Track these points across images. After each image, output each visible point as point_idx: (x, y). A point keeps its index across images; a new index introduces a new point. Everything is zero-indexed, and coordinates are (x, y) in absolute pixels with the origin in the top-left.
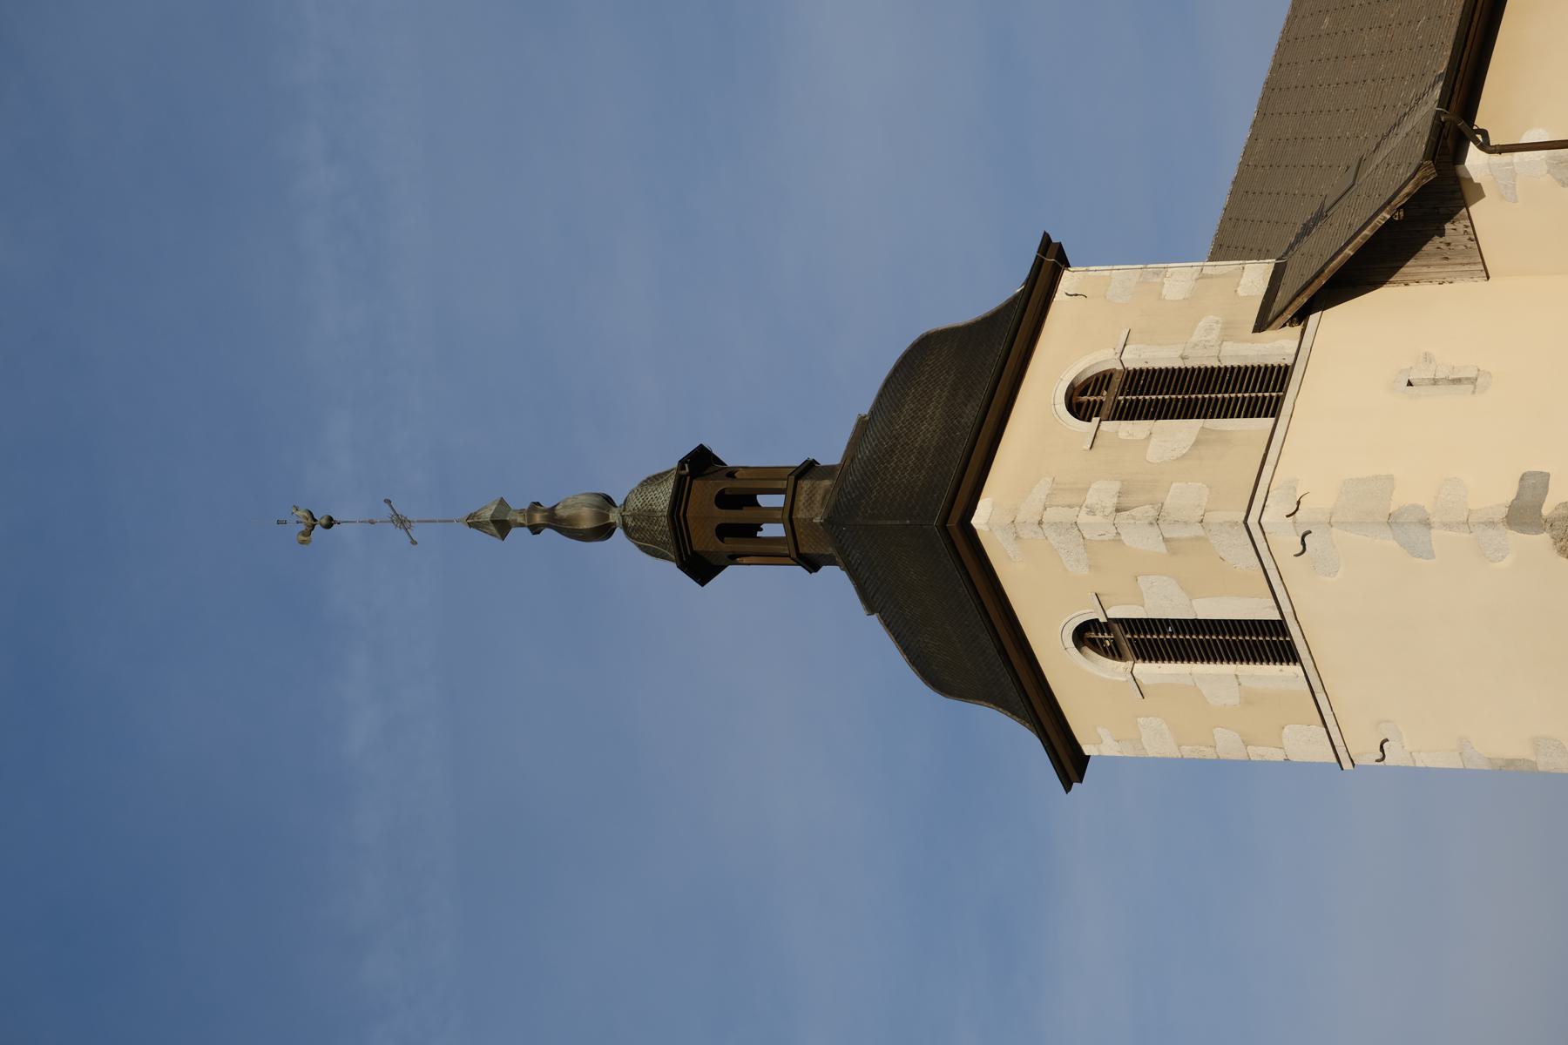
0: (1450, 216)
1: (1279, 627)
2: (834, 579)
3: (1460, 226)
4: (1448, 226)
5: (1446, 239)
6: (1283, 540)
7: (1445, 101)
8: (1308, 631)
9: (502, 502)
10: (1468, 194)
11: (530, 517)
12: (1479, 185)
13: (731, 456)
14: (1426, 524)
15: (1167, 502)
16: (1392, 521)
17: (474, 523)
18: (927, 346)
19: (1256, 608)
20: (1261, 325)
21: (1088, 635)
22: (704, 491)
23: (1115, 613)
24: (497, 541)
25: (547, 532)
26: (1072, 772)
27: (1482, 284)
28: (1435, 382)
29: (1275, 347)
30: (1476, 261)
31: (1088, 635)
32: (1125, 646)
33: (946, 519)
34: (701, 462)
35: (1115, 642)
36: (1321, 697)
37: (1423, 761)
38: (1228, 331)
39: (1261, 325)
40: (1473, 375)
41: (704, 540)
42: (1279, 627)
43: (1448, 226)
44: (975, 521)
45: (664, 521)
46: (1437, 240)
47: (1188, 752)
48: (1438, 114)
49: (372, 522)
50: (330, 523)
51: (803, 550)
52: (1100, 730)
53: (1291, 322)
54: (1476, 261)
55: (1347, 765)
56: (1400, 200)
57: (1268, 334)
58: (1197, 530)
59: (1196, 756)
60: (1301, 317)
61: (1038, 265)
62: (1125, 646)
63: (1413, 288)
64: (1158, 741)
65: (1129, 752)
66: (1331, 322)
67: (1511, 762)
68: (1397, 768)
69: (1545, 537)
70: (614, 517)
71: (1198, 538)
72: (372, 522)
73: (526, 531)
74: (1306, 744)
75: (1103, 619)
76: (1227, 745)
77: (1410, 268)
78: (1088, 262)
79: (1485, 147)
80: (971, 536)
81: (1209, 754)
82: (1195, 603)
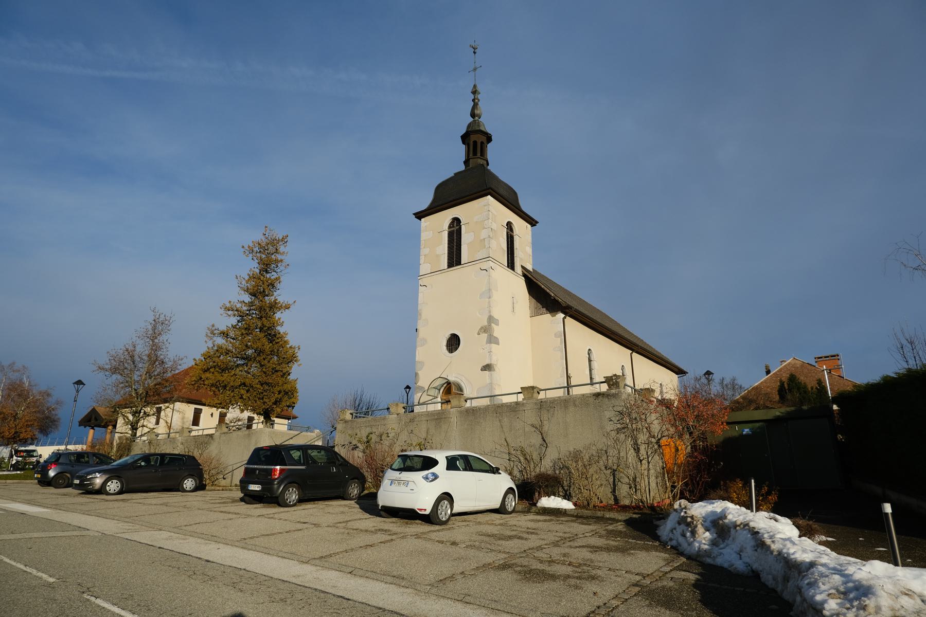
0: (547, 309)
1: (460, 264)
2: (462, 168)
3: (545, 311)
4: (545, 309)
5: (541, 308)
6: (485, 265)
7: (576, 311)
8: (456, 270)
9: (480, 93)
10: (553, 313)
11: (477, 99)
12: (555, 316)
13: (490, 147)
14: (490, 298)
15: (493, 240)
16: (490, 290)
17: (475, 86)
18: (515, 193)
19: (464, 258)
20: (523, 267)
21: (456, 222)
22: (484, 139)
23: (463, 227)
24: (471, 91)
25: (473, 103)
26: (418, 215)
27: (529, 315)
28: (513, 303)
29: (518, 269)
30: (535, 314)
31: (456, 222)
32: (452, 229)
33: (492, 189)
34: (489, 139)
35: (453, 227)
36: (439, 272)
37: (420, 295)
38: (521, 259)
39: (523, 267)
40: (515, 311)
41: (473, 138)
42: (460, 264)
43: (545, 309)
44: (489, 197)
45: (478, 129)
46: (541, 306)
47: (422, 242)
48: (574, 308)
49: (475, 62)
50: (475, 53)
51: (471, 160)
52: (428, 222)
53: (523, 273)
54: (535, 314)
55: (419, 278)
56: (557, 298)
57: (521, 268)
58: (487, 246)
59: (421, 244)
60: (524, 275)
61: (533, 220)
62: (452, 229)
63: (528, 301)
64: (424, 236)
65: (422, 229)
66: (522, 282)
67: (420, 315)
68: (418, 288)
69: (486, 324)
70: (477, 118)
71: (485, 246)
72: (475, 62)
73: (473, 98)
74: (424, 268)
75: (461, 224)
76: (424, 251)
77: (533, 300)
78: (532, 231)
79: (565, 318)
80: (486, 195)
81: (422, 247)
82: (466, 245)
